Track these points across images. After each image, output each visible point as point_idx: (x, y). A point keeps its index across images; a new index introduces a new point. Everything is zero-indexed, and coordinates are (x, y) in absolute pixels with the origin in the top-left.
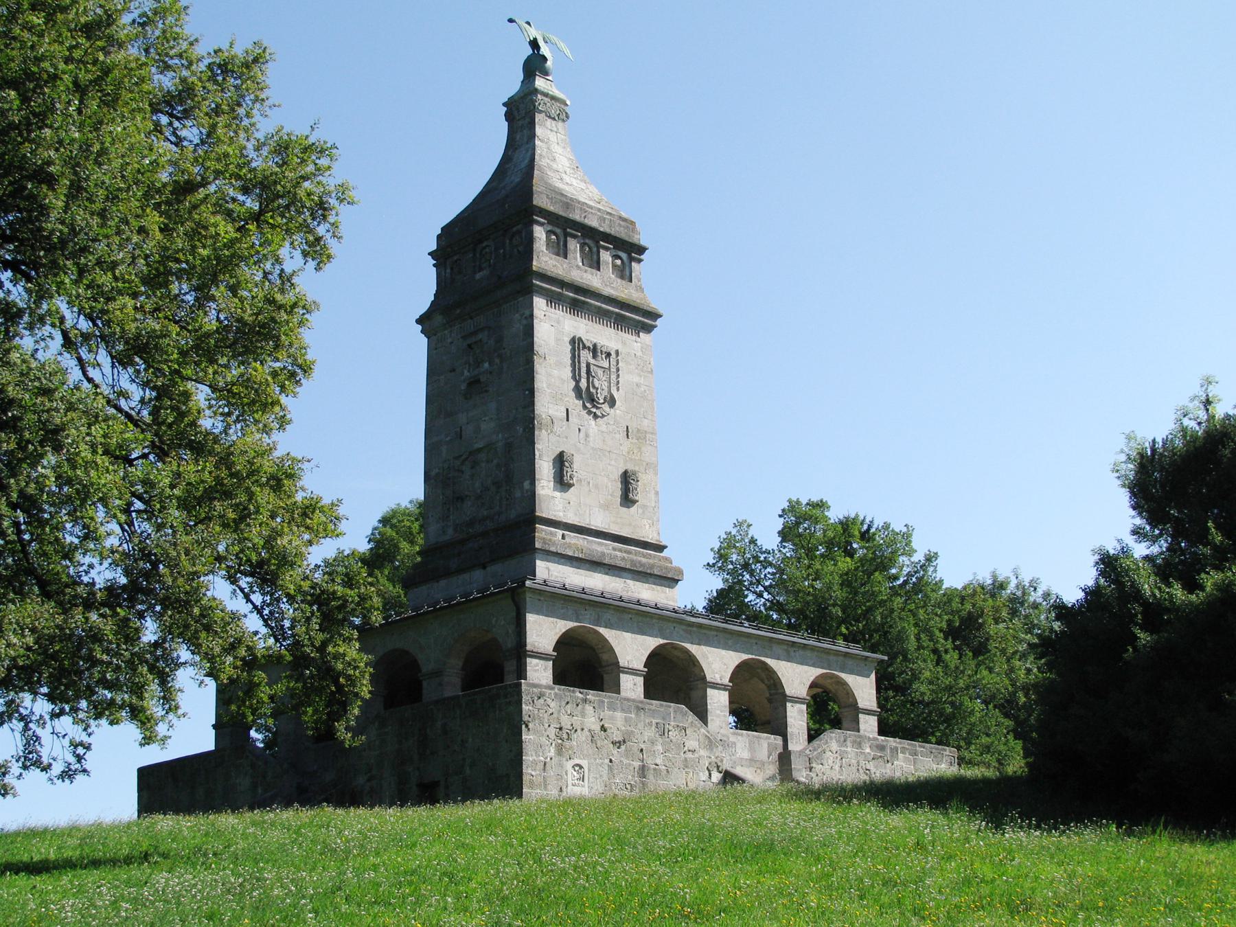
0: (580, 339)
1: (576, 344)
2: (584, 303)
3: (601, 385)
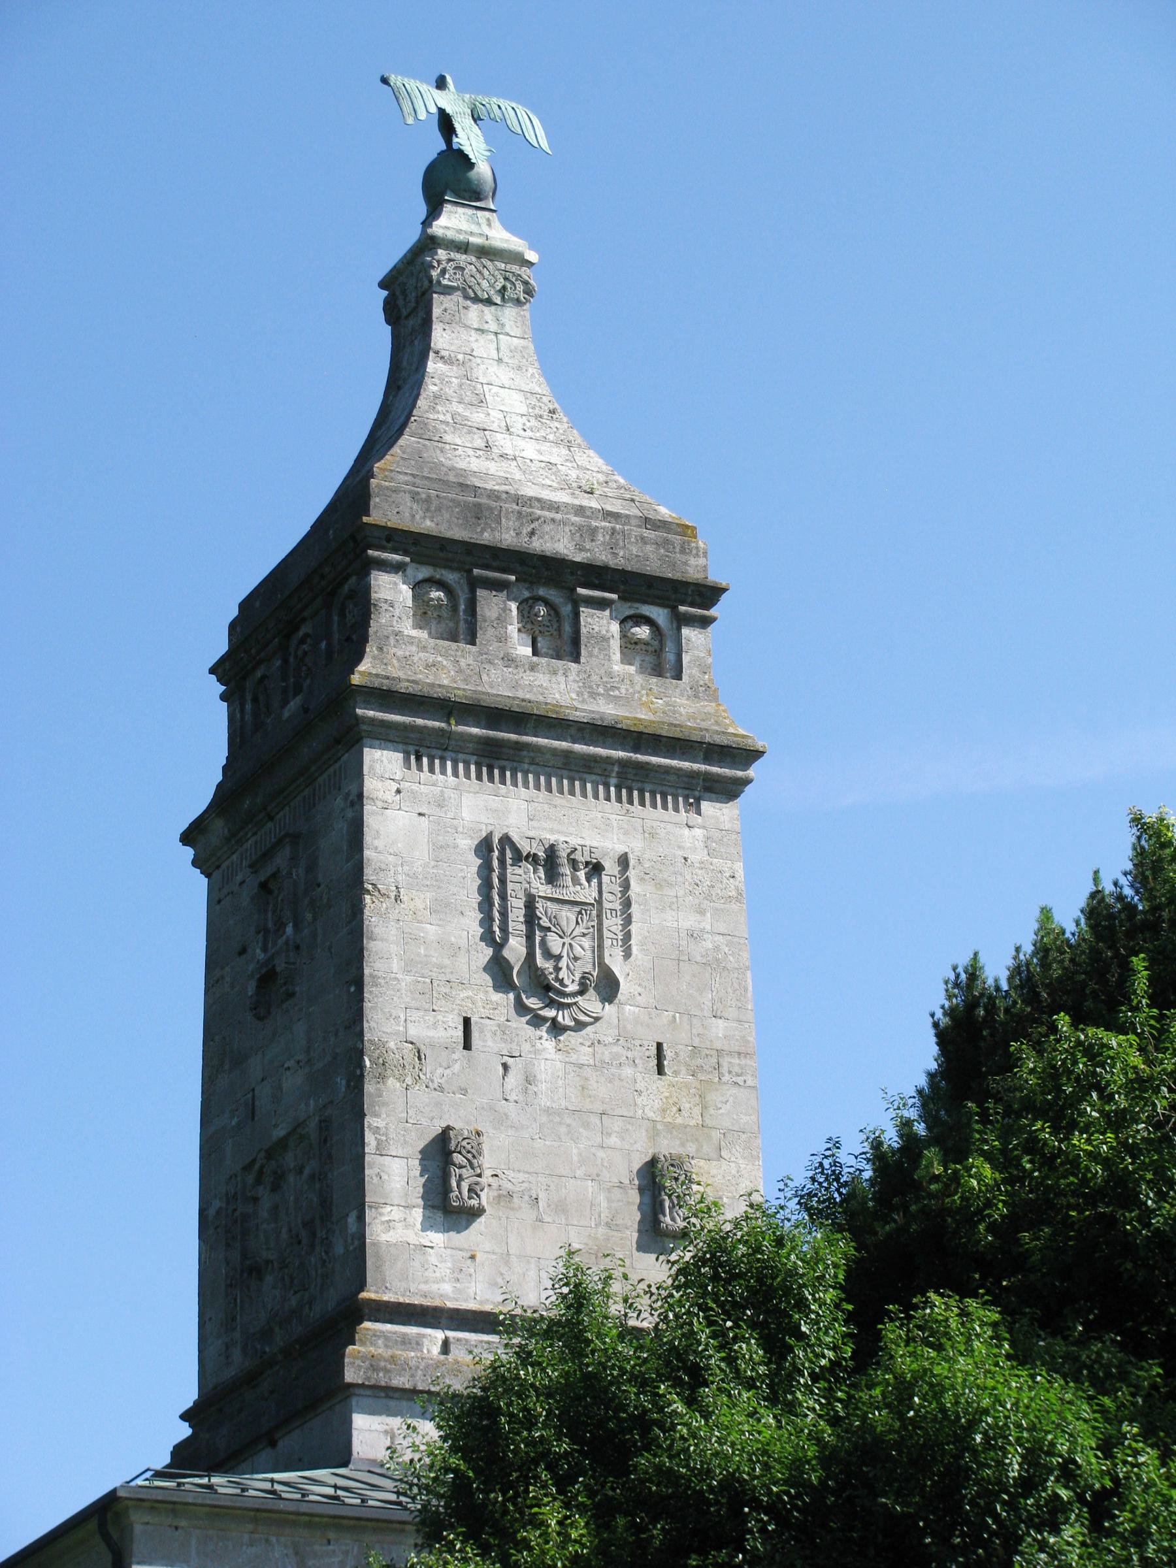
0: (506, 840)
1: (496, 854)
2: (519, 747)
3: (572, 952)
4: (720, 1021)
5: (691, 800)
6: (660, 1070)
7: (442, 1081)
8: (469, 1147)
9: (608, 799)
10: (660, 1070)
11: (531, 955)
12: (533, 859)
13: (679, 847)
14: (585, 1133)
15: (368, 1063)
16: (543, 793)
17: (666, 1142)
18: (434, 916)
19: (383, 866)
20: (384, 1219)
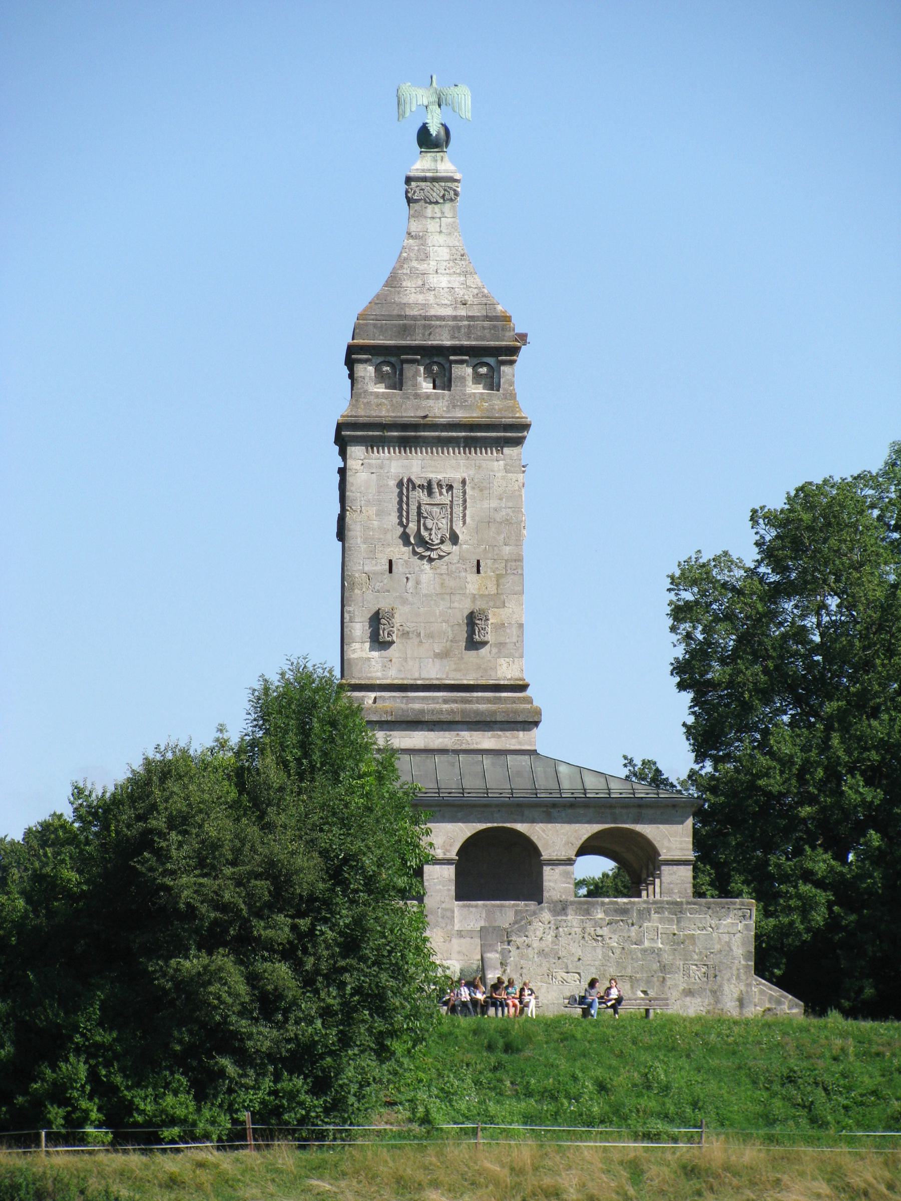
0: (410, 480)
1: (405, 486)
2: (416, 437)
3: (437, 527)
6: (478, 572)
10: (478, 572)
12: (421, 487)
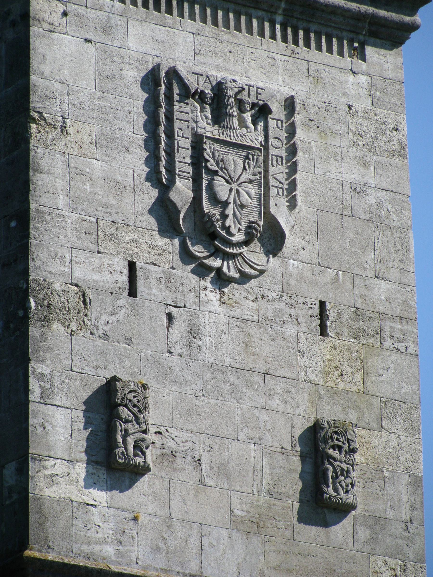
0: (173, 74)
1: (162, 87)
3: (238, 197)
4: (382, 283)
5: (356, 45)
7: (107, 328)
8: (135, 400)
9: (273, 37)
10: (323, 331)
11: (197, 201)
12: (200, 96)
13: (344, 94)
14: (249, 393)
15: (33, 304)
16: (209, 28)
17: (328, 407)
18: (100, 151)
19: (50, 95)
20: (48, 472)
